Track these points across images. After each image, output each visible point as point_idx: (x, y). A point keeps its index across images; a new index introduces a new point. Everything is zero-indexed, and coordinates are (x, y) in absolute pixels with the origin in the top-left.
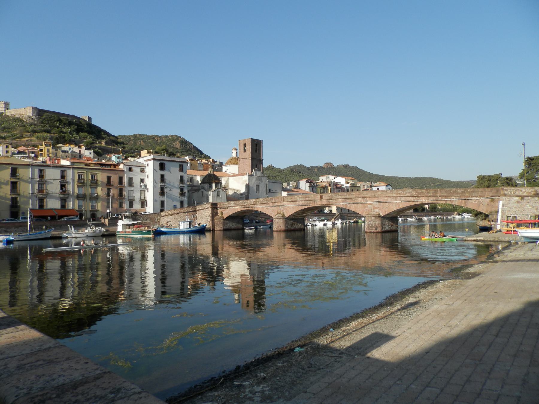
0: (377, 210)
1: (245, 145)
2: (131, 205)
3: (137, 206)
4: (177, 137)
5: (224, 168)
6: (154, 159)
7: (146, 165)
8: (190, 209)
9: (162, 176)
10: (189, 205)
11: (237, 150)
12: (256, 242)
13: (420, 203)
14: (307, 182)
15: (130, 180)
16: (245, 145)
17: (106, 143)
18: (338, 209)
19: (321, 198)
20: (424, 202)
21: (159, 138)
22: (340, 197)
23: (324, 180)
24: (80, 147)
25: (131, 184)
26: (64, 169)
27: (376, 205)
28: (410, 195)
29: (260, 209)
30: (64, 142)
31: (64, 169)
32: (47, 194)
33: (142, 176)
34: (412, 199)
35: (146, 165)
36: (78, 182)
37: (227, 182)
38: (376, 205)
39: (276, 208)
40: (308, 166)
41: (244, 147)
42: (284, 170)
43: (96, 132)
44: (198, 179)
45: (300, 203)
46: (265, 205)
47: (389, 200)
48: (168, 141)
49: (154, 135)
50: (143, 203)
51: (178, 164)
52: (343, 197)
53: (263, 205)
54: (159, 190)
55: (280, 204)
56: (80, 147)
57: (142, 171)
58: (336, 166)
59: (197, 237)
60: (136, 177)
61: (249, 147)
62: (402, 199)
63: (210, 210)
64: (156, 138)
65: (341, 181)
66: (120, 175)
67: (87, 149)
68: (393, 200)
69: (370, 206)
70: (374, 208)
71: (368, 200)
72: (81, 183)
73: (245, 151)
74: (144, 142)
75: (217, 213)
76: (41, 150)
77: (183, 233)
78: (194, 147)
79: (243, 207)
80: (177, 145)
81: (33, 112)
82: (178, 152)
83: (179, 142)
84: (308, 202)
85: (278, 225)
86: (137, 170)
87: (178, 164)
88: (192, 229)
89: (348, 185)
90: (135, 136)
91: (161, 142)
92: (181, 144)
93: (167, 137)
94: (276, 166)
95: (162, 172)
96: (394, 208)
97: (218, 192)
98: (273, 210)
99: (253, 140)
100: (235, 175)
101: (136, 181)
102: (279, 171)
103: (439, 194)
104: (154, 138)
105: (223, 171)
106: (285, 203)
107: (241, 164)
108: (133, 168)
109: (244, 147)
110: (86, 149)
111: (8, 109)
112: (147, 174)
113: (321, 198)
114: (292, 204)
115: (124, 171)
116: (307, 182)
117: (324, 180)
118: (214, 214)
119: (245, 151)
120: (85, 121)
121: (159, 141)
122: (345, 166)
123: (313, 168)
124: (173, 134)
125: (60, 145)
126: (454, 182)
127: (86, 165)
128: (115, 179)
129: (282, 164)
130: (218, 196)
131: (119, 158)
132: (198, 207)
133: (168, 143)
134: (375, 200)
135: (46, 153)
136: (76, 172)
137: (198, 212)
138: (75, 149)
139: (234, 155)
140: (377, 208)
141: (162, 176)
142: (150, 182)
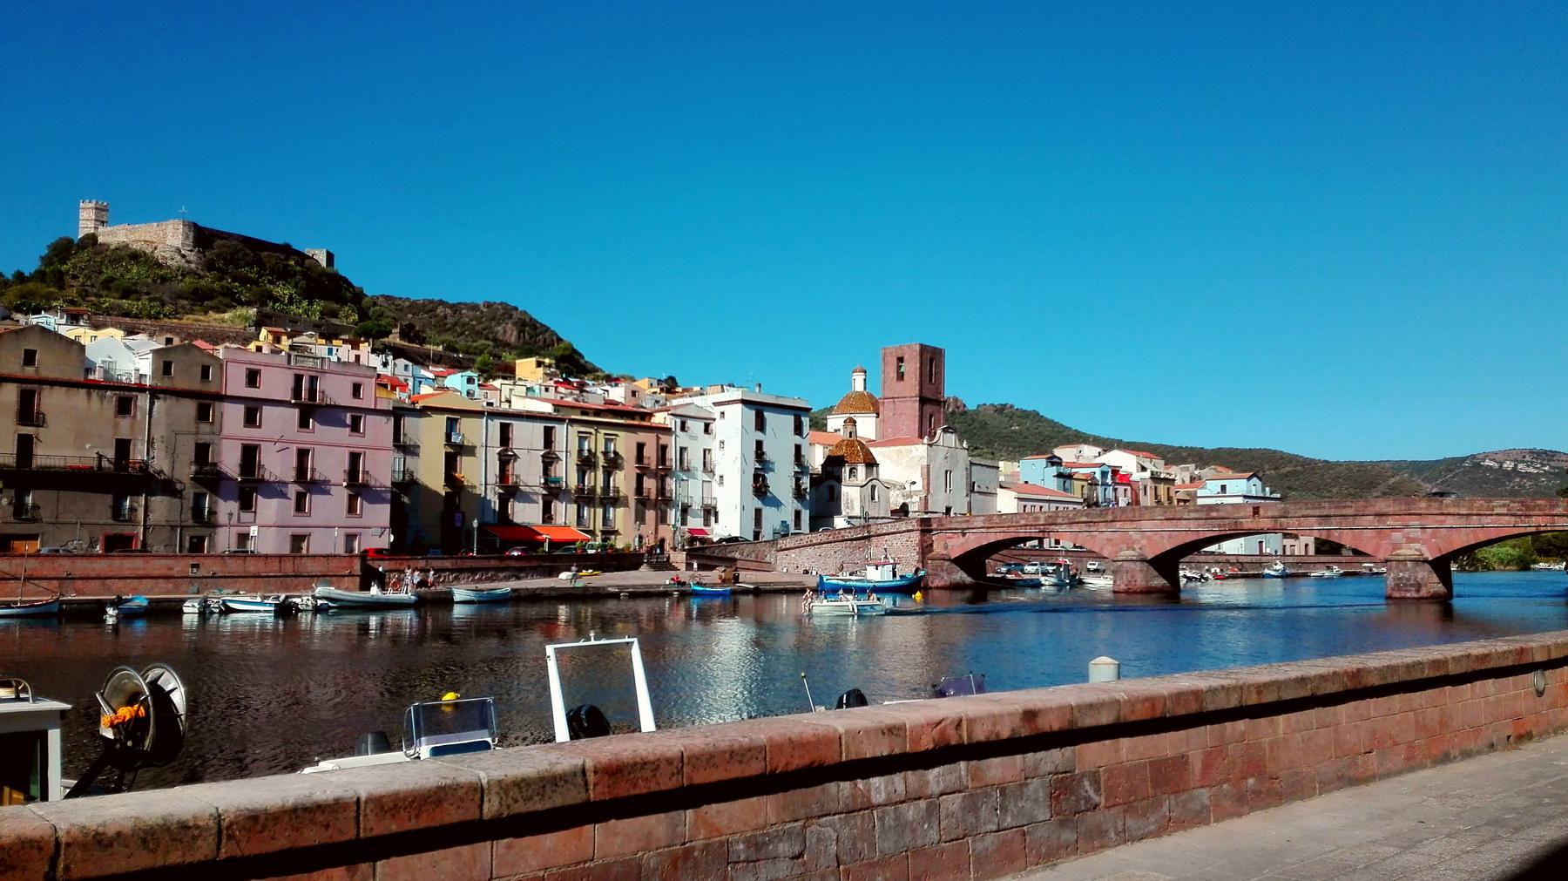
0: (1418, 546)
4: (508, 311)
6: (744, 402)
7: (717, 416)
9: (759, 444)
12: (852, 647)
16: (901, 360)
21: (448, 311)
27: (1416, 533)
33: (705, 441)
35: (717, 416)
38: (1416, 533)
45: (1192, 525)
46: (1083, 527)
47: (1450, 521)
48: (479, 320)
49: (431, 302)
50: (710, 512)
52: (1318, 512)
55: (1128, 525)
58: (971, 406)
60: (693, 442)
61: (912, 368)
62: (1485, 520)
68: (1461, 522)
69: (1397, 536)
70: (1410, 540)
71: (1390, 522)
72: (586, 463)
73: (901, 377)
83: (515, 324)
86: (696, 427)
88: (898, 582)
91: (456, 324)
92: (521, 332)
93: (475, 307)
98: (1109, 540)
99: (924, 349)
104: (433, 310)
106: (1147, 525)
110: (373, 351)
112: (718, 439)
114: (1168, 526)
119: (901, 377)
121: (450, 320)
122: (1001, 409)
124: (496, 298)
126: (1338, 464)
127: (584, 413)
128: (650, 452)
131: (470, 380)
133: (479, 328)
134: (1414, 522)
136: (497, 423)
141: (759, 444)
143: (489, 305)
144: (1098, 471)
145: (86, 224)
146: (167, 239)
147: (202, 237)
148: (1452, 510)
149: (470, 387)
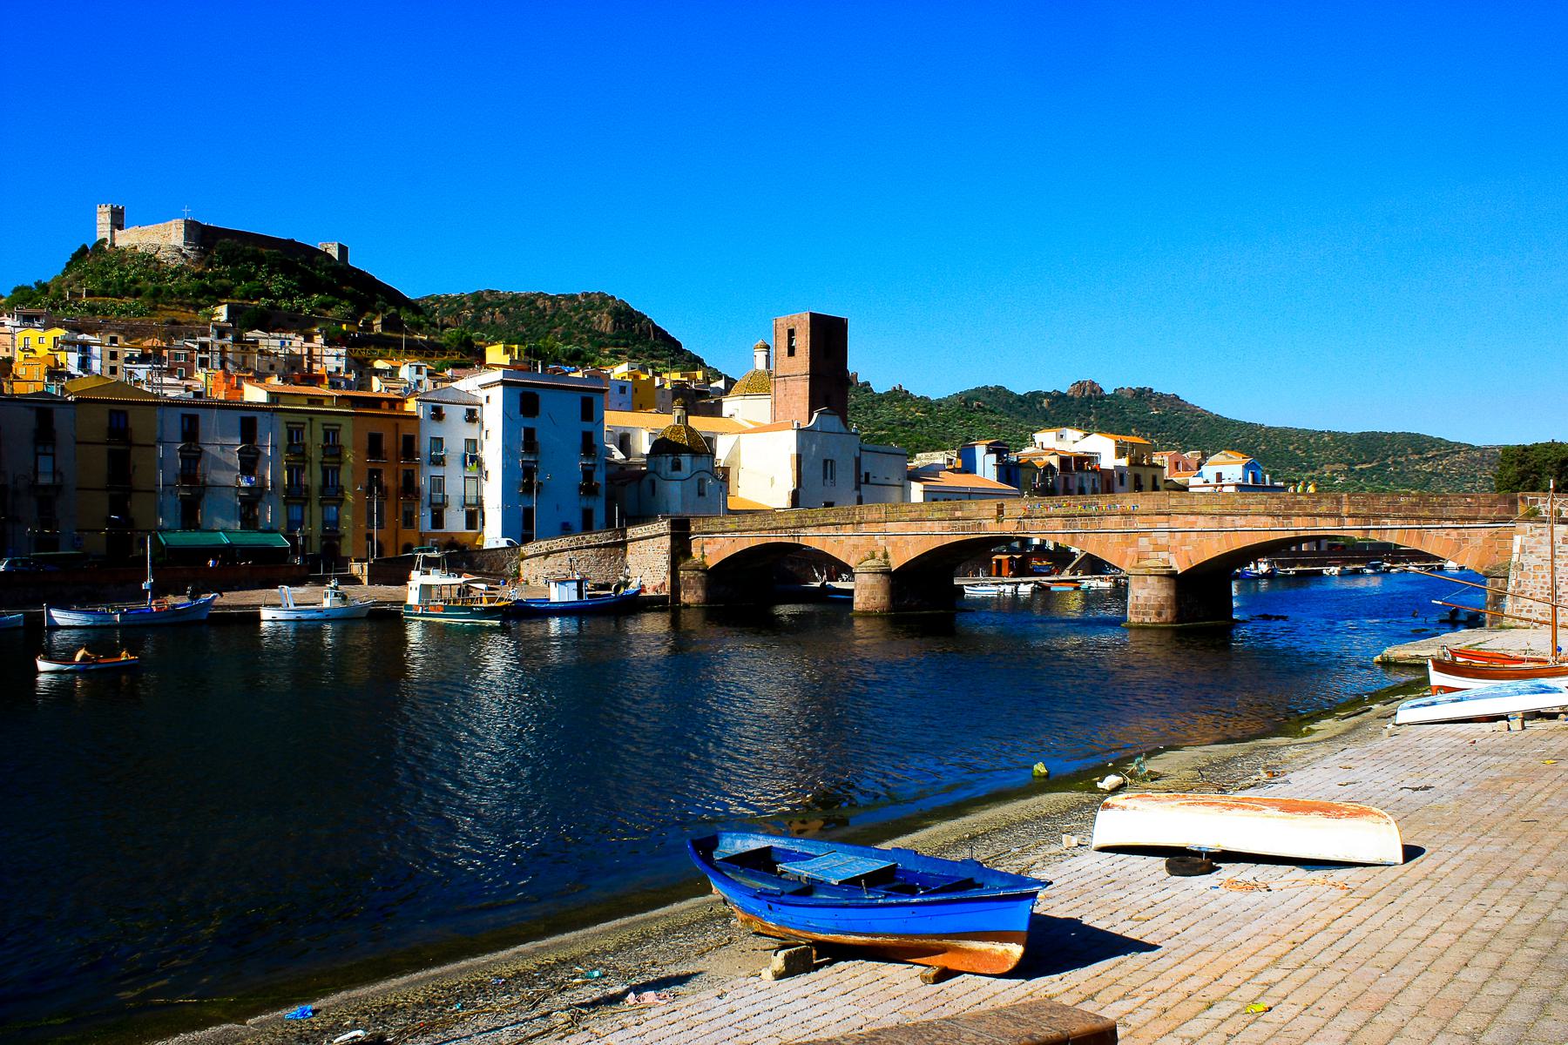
0: (1164, 555)
1: (791, 333)
2: (438, 521)
3: (455, 522)
4: (604, 298)
5: (729, 405)
6: (503, 383)
8: (603, 537)
10: (609, 524)
11: (768, 347)
13: (1292, 535)
14: (989, 452)
15: (438, 442)
16: (791, 333)
17: (384, 323)
18: (1056, 545)
19: (1000, 512)
20: (1302, 534)
21: (548, 303)
22: (1057, 511)
23: (1051, 444)
24: (309, 338)
25: (439, 461)
26: (587, 394)
27: (1163, 539)
28: (1261, 508)
29: (816, 544)
30: (269, 321)
31: (587, 394)
32: (205, 486)
33: (471, 432)
34: (1265, 521)
36: (288, 450)
37: (735, 452)
38: (1163, 539)
39: (862, 540)
40: (1020, 390)
41: (790, 341)
42: (939, 403)
43: (366, 292)
44: (643, 445)
45: (937, 527)
46: (831, 530)
48: (575, 309)
50: (474, 516)
51: (578, 397)
53: (823, 531)
54: (519, 478)
55: (874, 528)
56: (309, 338)
57: (471, 417)
58: (1109, 391)
59: (605, 626)
60: (455, 433)
61: (803, 342)
63: (666, 542)
64: (540, 303)
65: (1104, 450)
66: (406, 430)
67: (329, 343)
69: (1144, 541)
70: (1158, 548)
71: (1139, 524)
73: (791, 352)
74: (505, 313)
75: (688, 554)
76: (204, 347)
77: (563, 611)
78: (657, 329)
79: (764, 533)
80: (605, 323)
81: (188, 235)
82: (606, 346)
83: (609, 313)
84: (960, 523)
85: (866, 592)
86: (455, 414)
87: (578, 397)
89: (1124, 462)
90: (477, 297)
93: (573, 298)
94: (917, 392)
95: (529, 423)
96: (1215, 547)
97: (701, 481)
98: (856, 546)
99: (815, 318)
100: (760, 429)
101: (454, 445)
102: (927, 405)
103: (1345, 510)
104: (533, 302)
105: (725, 413)
107: (780, 394)
108: (446, 409)
109: (790, 341)
111: (120, 227)
113: (1000, 512)
114: (913, 528)
115: (417, 417)
116: (989, 452)
117: (1051, 444)
118: (680, 550)
119: (791, 352)
120: (330, 257)
123: (1035, 396)
125: (257, 333)
129: (937, 382)
130: (701, 494)
132: (632, 532)
134: (1161, 522)
135: (217, 357)
137: (630, 546)
138: (297, 344)
139: (760, 364)
140: (1167, 548)
141: (529, 433)
142: (493, 454)
143: (586, 295)
144: (1055, 462)
145: (103, 229)
146: (164, 238)
147: (199, 234)
148: (1204, 509)
149: (113, 363)
